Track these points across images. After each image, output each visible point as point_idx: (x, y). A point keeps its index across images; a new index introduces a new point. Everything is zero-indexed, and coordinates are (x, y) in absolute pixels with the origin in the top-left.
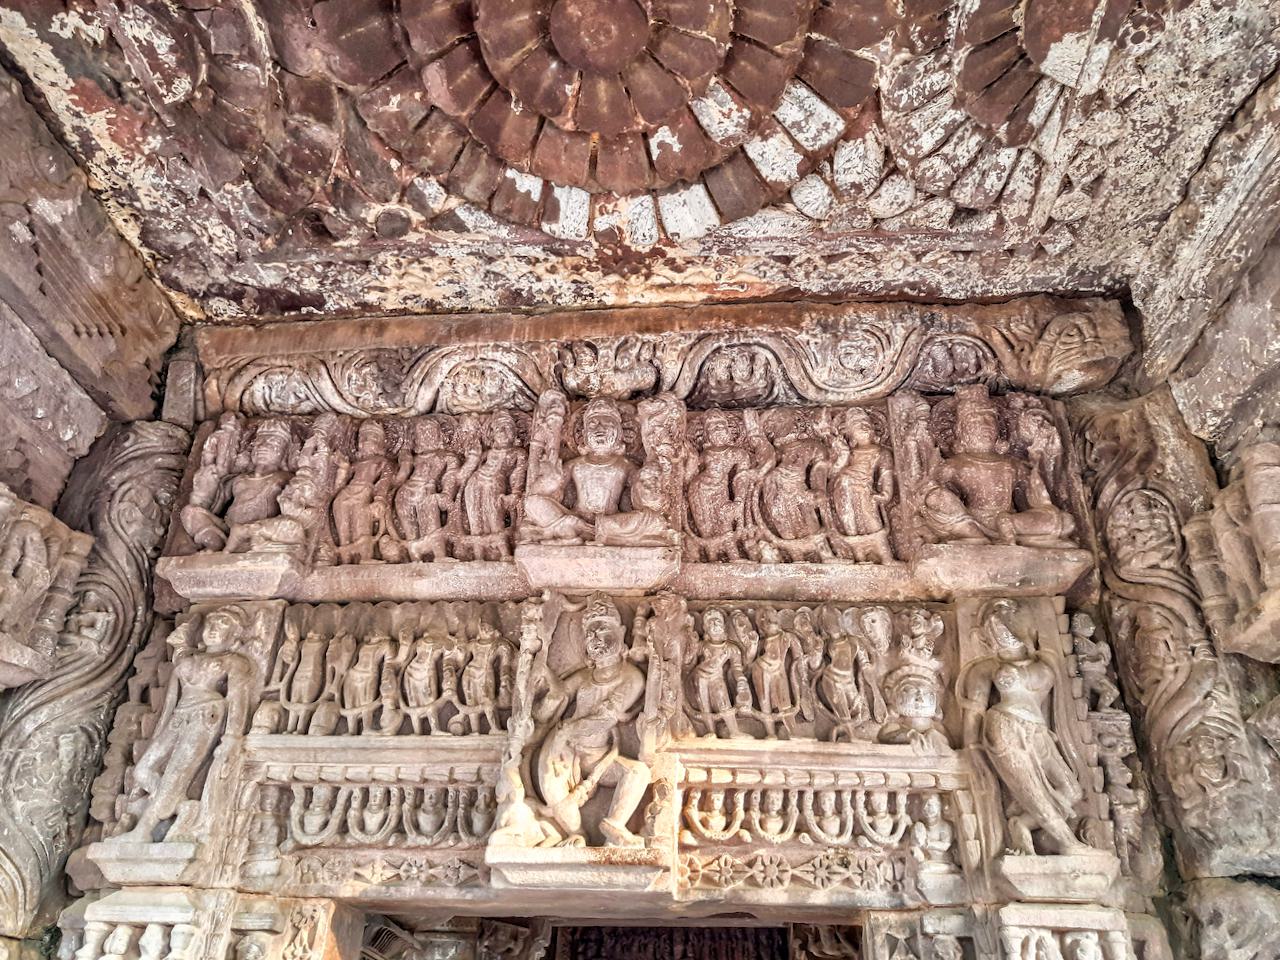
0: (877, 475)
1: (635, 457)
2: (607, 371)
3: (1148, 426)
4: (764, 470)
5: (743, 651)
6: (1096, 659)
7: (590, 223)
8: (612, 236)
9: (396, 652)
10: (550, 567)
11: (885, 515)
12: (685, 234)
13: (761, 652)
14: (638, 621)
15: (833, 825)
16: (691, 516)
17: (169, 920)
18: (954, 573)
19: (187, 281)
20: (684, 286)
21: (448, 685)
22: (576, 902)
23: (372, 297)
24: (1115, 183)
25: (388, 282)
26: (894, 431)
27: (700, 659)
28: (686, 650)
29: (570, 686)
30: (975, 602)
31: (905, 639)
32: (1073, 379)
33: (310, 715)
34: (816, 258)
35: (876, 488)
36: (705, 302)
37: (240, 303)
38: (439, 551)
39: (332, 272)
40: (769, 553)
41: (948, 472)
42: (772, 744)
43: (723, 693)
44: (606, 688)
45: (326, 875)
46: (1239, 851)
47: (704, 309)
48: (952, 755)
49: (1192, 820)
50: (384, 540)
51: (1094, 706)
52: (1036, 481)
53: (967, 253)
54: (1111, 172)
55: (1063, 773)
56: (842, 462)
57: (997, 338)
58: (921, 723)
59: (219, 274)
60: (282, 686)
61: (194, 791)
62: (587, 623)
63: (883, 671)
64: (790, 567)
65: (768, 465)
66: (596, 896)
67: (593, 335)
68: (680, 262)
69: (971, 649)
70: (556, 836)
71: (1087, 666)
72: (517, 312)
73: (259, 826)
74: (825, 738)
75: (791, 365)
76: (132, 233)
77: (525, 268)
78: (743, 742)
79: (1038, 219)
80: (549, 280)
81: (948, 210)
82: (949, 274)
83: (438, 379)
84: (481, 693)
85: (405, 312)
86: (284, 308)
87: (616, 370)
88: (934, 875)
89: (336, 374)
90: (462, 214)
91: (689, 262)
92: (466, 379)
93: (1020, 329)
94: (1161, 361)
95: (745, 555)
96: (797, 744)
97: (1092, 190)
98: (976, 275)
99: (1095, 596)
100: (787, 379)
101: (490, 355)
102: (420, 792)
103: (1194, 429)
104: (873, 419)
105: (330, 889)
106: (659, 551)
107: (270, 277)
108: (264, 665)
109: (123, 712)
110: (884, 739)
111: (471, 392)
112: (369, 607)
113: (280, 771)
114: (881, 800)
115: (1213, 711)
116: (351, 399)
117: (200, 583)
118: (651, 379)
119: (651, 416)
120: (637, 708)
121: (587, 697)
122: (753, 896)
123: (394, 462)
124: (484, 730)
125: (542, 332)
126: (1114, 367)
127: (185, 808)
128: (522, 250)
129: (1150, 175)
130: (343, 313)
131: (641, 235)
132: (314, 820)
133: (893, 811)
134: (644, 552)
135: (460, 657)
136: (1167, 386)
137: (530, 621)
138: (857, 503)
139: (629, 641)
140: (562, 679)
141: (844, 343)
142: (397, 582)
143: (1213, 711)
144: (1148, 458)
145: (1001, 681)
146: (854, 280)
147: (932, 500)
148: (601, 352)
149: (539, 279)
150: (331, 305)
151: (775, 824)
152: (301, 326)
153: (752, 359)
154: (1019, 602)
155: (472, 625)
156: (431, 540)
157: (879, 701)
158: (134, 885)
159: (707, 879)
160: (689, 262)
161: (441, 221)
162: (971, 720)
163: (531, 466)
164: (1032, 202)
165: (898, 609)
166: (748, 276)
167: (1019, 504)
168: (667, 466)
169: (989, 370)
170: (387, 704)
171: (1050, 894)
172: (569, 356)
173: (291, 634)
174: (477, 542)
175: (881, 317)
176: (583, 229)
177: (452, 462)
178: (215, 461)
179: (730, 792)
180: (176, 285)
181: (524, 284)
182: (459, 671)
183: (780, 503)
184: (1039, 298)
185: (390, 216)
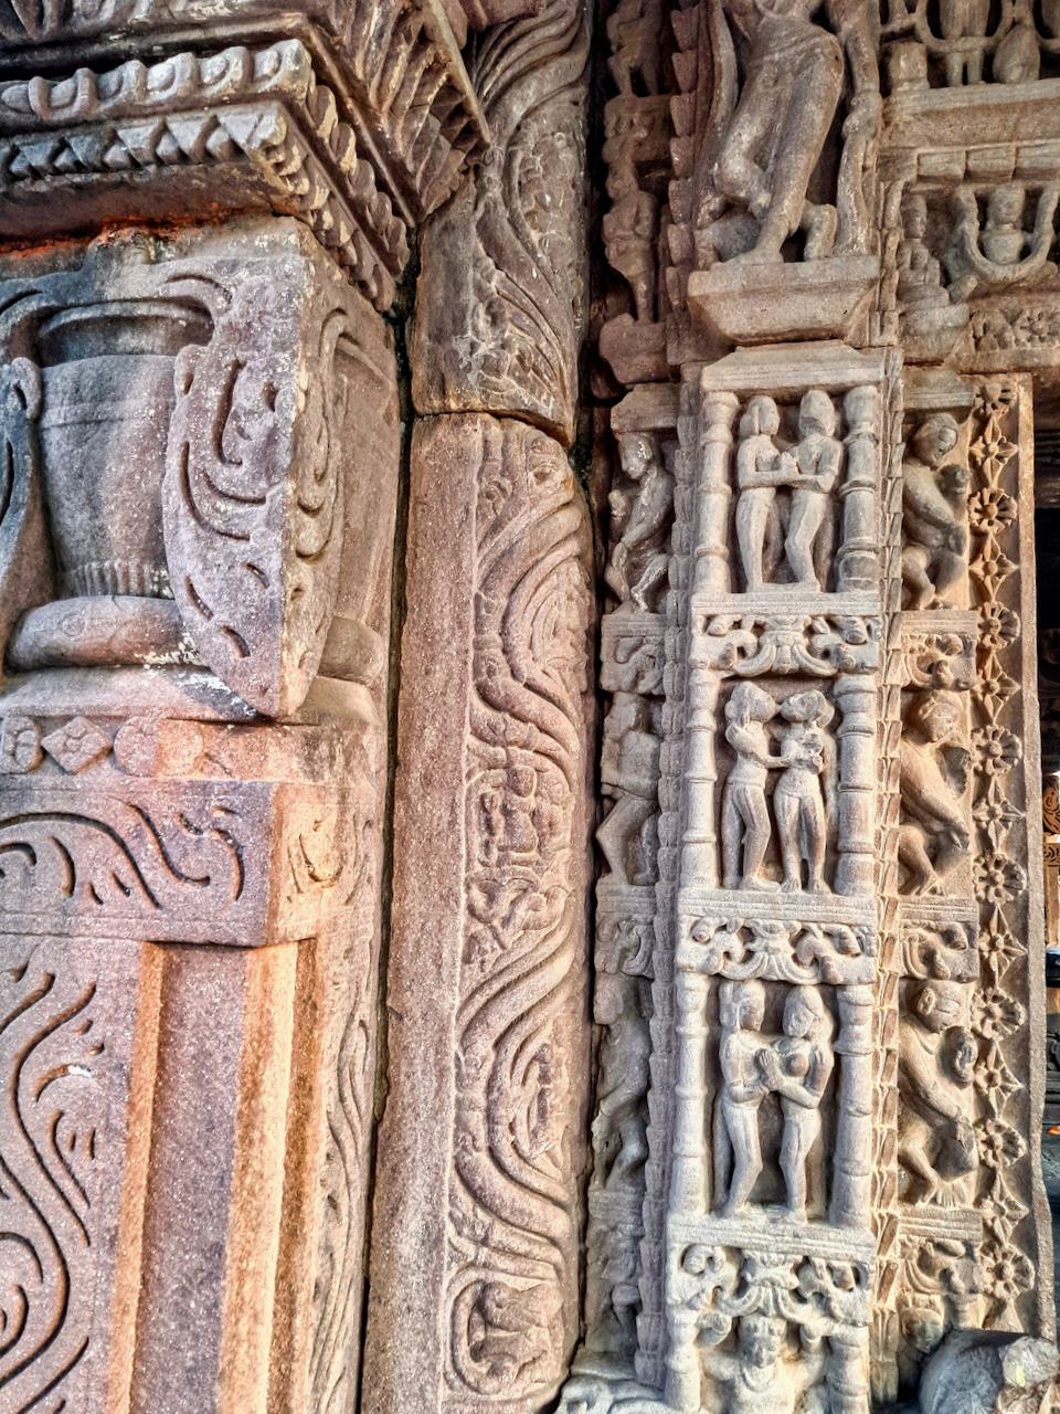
45: (1024, 336)
61: (824, 189)
73: (908, 258)
105: (1032, 355)
109: (613, 112)
113: (941, 160)
127: (824, 216)
132: (1014, 240)
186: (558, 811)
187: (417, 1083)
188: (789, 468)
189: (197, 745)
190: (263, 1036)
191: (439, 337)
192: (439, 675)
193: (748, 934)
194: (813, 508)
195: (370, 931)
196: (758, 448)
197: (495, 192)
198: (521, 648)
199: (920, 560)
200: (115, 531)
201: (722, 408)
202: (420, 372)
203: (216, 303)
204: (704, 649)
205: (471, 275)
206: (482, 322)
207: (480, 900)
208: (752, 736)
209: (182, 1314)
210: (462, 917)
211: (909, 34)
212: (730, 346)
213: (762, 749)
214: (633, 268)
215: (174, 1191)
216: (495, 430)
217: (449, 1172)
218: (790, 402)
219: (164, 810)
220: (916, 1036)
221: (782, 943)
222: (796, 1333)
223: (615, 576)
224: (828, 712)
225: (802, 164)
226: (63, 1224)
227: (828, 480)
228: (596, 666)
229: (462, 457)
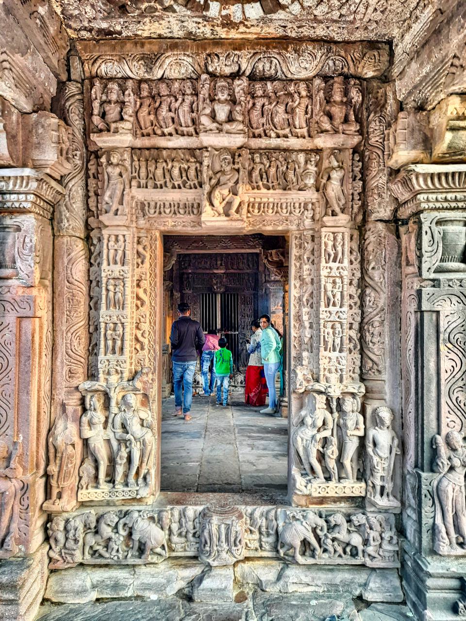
0: (307, 107)
1: (233, 101)
2: (223, 66)
3: (386, 94)
4: (273, 105)
5: (265, 166)
6: (357, 167)
7: (220, 12)
8: (227, 17)
9: (167, 165)
10: (207, 140)
11: (308, 122)
12: (252, 18)
13: (270, 166)
14: (236, 157)
15: (285, 211)
16: (250, 121)
17: (117, 234)
18: (324, 142)
19: (74, 25)
20: (249, 33)
21: (184, 175)
22: (221, 230)
23: (139, 33)
24: (390, 11)
25: (146, 28)
26: (314, 92)
27: (253, 168)
28: (249, 165)
29: (218, 175)
30: (329, 151)
31: (309, 162)
32: (370, 74)
33: (147, 183)
34: (295, 27)
35: (306, 113)
36: (256, 39)
37: (91, 33)
38: (174, 132)
39: (126, 24)
40: (273, 135)
41: (328, 108)
42: (271, 191)
43: (259, 178)
44: (228, 177)
46: (378, 214)
47: (256, 41)
48: (316, 193)
49: (370, 208)
50: (156, 128)
51: (354, 180)
52: (352, 113)
53: (343, 28)
54: (389, 8)
55: (342, 197)
56: (297, 103)
57: (349, 58)
58: (309, 185)
59: (86, 24)
60: (136, 174)
62: (222, 158)
63: (302, 171)
64: (279, 140)
65: (274, 104)
66: (227, 229)
67: (218, 51)
68: (249, 26)
69: (326, 164)
70: (217, 214)
71: (355, 169)
72: (190, 39)
74: (285, 189)
75: (284, 66)
76: (59, 10)
77: (195, 25)
78: (264, 191)
79: (366, 19)
80: (202, 29)
81: (338, 14)
82: (338, 33)
83: (165, 66)
84: (193, 178)
85: (150, 38)
86: (106, 35)
87: (226, 65)
88: (308, 222)
89: (130, 63)
90: (175, 7)
91: (252, 26)
92: (175, 66)
93: (357, 55)
94: (396, 71)
95: (266, 135)
96: (278, 191)
97: (382, 12)
98: (346, 34)
99: (362, 148)
100: (282, 70)
101: (183, 58)
102: (179, 204)
103: (398, 97)
104: (308, 87)
106: (242, 135)
107: (104, 25)
108: (129, 168)
110: (300, 190)
111: (176, 72)
112: (156, 151)
114: (297, 205)
115: (380, 181)
116: (135, 73)
117: (105, 142)
118: (237, 68)
119: (239, 86)
120: (237, 182)
121: (223, 179)
122: (264, 228)
123: (153, 98)
124: (196, 188)
125: (200, 49)
126: (382, 71)
127: (120, 207)
128: (195, 19)
129: (400, 9)
130: (128, 38)
131: (237, 17)
132: (152, 211)
133: (300, 208)
134: (237, 135)
135: (186, 167)
136: (394, 80)
137: (206, 157)
138: (300, 119)
139: (234, 163)
140: (216, 173)
141: (301, 58)
142: (162, 142)
143: (380, 181)
144: (384, 106)
145: (331, 174)
146: (306, 34)
147: (322, 119)
148: (221, 58)
149: (199, 28)
150: (124, 34)
151: (270, 211)
152: (113, 42)
153: (271, 63)
154: (340, 150)
155: (187, 157)
156: (170, 129)
157: (300, 179)
158: (111, 226)
159: (253, 225)
160: (252, 26)
161: (169, 9)
162: (322, 184)
163: (200, 103)
164: (365, 14)
165: (307, 152)
166: (272, 31)
167: (346, 120)
168: (244, 104)
169: (345, 70)
170: (168, 180)
171: (333, 225)
172: (209, 59)
173: (135, 158)
174: (185, 129)
175: (314, 48)
176: (217, 14)
177: (173, 99)
178: (96, 99)
179: (260, 204)
180: (70, 27)
181: (194, 30)
182: (186, 171)
183: (277, 118)
184: (365, 42)
185: (151, 7)
186: (81, 300)
187: (59, 340)
188: (116, 247)
189: (22, 290)
190: (34, 330)
191: (58, 223)
192: (60, 278)
193: (110, 317)
194: (120, 253)
195: (51, 318)
196: (112, 243)
197: (67, 199)
198: (74, 274)
199: (140, 261)
200: (7, 259)
201: (106, 237)
202: (55, 229)
203: (22, 226)
204: (103, 274)
205: (63, 213)
206: (66, 221)
207: (68, 313)
208: (111, 288)
209: (25, 365)
210: (66, 316)
211: (135, 178)
212: (107, 226)
213: (113, 290)
214: (94, 209)
215: (23, 350)
216: (69, 239)
217: (65, 353)
218: (117, 236)
219: (18, 299)
220: (138, 331)
221: (115, 318)
222: (117, 371)
223: (92, 261)
224: (122, 284)
225: (116, 200)
226: (7, 354)
227: (122, 249)
228: (89, 276)
229: (63, 243)
